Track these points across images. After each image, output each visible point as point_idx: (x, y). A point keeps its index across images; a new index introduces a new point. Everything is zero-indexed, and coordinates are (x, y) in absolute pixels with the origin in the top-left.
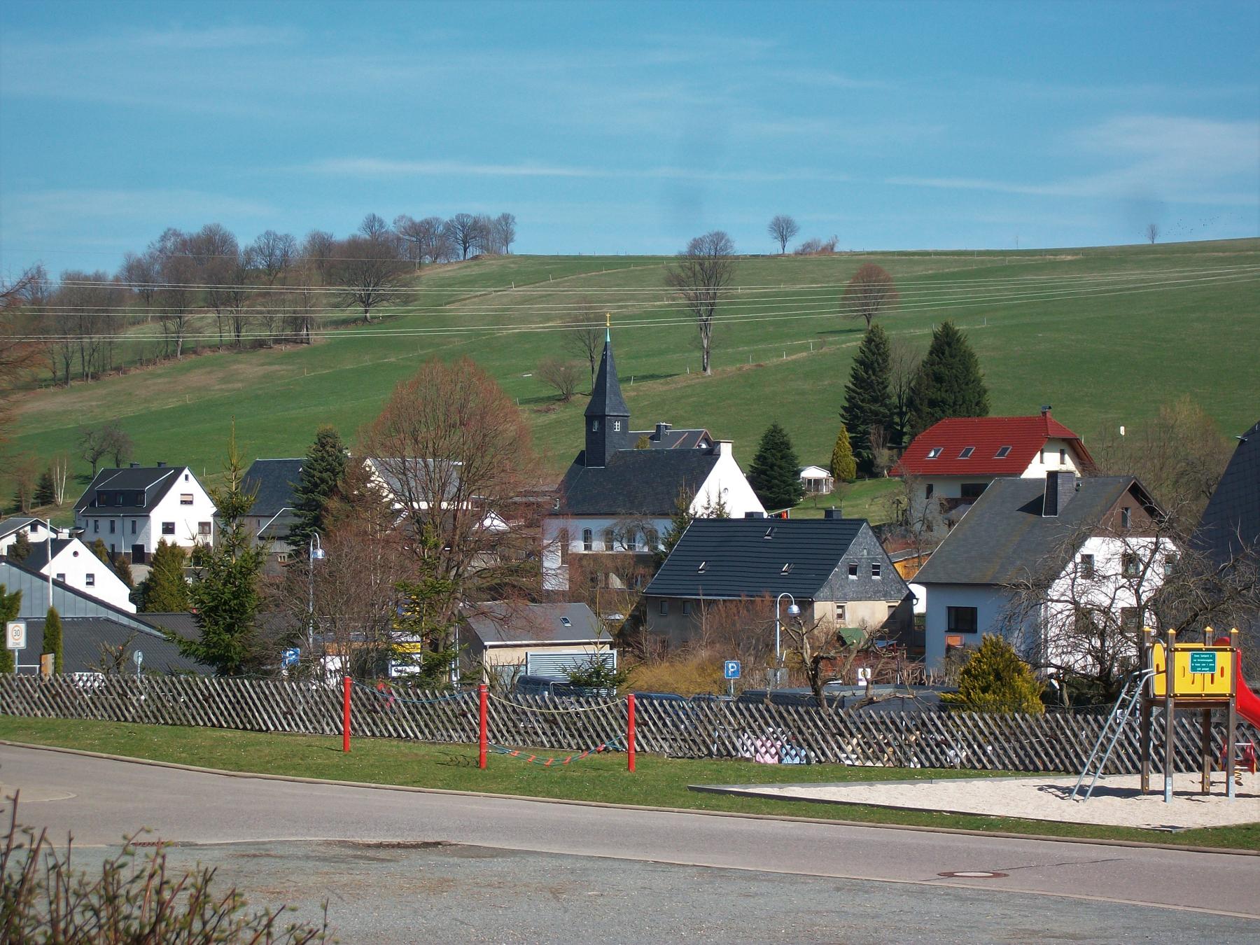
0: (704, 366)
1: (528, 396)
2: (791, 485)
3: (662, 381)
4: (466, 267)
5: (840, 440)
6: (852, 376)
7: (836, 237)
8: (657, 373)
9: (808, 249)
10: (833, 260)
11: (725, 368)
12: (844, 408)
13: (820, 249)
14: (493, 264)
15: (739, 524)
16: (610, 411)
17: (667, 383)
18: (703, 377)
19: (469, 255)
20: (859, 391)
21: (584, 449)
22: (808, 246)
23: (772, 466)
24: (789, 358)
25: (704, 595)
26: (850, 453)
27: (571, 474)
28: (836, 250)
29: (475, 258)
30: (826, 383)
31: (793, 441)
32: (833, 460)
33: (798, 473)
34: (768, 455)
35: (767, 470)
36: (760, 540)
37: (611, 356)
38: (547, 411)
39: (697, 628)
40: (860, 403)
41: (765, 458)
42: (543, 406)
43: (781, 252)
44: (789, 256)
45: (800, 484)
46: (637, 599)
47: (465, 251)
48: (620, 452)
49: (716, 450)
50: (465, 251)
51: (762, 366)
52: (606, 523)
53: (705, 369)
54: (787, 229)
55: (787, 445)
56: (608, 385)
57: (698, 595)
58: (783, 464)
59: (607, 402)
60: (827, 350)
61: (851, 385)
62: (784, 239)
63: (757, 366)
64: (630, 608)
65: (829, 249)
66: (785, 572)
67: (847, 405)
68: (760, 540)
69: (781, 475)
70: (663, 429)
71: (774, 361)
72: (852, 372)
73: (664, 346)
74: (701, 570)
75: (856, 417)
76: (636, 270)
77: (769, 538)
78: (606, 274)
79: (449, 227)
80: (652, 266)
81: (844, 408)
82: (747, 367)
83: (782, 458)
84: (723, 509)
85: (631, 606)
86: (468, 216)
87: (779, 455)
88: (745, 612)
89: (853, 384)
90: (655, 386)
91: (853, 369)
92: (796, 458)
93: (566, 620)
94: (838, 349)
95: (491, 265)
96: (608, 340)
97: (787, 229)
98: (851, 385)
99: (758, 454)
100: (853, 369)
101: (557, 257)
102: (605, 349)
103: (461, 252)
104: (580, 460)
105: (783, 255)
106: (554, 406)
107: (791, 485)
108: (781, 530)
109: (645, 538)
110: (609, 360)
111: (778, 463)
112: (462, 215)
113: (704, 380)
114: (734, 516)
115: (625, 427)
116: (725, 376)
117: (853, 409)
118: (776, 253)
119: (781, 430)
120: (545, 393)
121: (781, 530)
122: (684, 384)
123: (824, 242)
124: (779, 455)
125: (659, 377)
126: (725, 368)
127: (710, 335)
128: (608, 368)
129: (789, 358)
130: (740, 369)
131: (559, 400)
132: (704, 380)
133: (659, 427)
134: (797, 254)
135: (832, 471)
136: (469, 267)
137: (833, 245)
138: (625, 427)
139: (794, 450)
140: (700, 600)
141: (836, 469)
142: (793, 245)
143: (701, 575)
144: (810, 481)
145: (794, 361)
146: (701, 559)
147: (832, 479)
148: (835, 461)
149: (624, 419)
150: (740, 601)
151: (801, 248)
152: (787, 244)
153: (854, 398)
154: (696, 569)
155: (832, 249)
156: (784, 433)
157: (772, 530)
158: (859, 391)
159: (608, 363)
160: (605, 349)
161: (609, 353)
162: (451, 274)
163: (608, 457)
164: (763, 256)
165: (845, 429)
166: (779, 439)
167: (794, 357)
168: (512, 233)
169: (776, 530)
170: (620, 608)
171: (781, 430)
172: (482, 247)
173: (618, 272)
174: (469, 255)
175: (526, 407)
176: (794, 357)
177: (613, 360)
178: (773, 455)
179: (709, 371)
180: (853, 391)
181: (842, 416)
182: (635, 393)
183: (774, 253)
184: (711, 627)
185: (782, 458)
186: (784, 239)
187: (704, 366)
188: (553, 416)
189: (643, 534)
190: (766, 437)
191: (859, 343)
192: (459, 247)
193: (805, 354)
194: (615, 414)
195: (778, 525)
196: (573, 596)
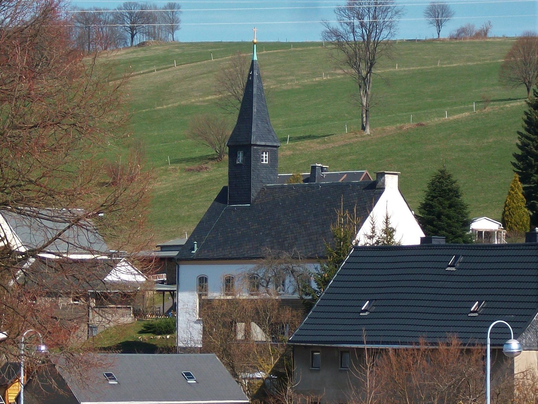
0: (363, 125)
1: (179, 157)
2: (460, 236)
3: (319, 140)
4: (132, 52)
5: (513, 190)
6: (526, 122)
7: (490, 22)
8: (314, 134)
9: (463, 34)
10: (487, 42)
11: (385, 128)
12: (517, 156)
13: (474, 34)
14: (157, 50)
15: (413, 252)
16: (256, 140)
17: (325, 142)
18: (362, 137)
19: (136, 42)
20: (532, 137)
21: (227, 184)
22: (463, 31)
23: (439, 216)
24: (451, 118)
25: (368, 343)
26: (523, 205)
27: (212, 212)
28: (489, 35)
29: (142, 44)
30: (491, 140)
31: (462, 189)
32: (504, 212)
33: (467, 224)
34: (435, 203)
35: (433, 220)
36: (441, 272)
37: (259, 77)
38: (200, 170)
39: (359, 385)
40: (534, 150)
41: (431, 206)
42: (196, 165)
43: (436, 37)
44: (443, 41)
45: (470, 236)
46: (281, 350)
47: (132, 37)
48: (268, 188)
49: (380, 184)
50: (132, 37)
51: (422, 125)
52: (248, 268)
53: (364, 128)
54: (442, 14)
55: (456, 193)
56: (255, 110)
57: (362, 343)
58: (452, 212)
59: (254, 130)
60: (491, 110)
61: (525, 132)
62: (439, 24)
63: (418, 125)
64: (273, 361)
65: (483, 34)
66: (474, 312)
67: (519, 152)
68: (441, 272)
69: (449, 226)
70: (318, 171)
71: (434, 121)
72: (525, 117)
73: (322, 116)
74: (365, 311)
75: (531, 166)
76: (296, 51)
77: (453, 269)
78: (266, 54)
79: (118, 18)
80: (311, 48)
81: (517, 156)
82: (407, 126)
83: (450, 206)
84: (392, 237)
85: (275, 359)
86: (136, 4)
87: (447, 203)
88: (424, 362)
89: (526, 130)
90: (312, 145)
91: (526, 113)
92: (465, 207)
93: (189, 376)
94: (502, 109)
95: (157, 50)
96: (255, 58)
97: (442, 14)
98: (525, 132)
99: (424, 202)
100: (526, 113)
101: (221, 43)
102: (252, 69)
103: (129, 41)
104: (222, 197)
105: (438, 39)
106: (206, 165)
107: (460, 236)
108: (468, 259)
109: (295, 283)
110: (255, 81)
111: (446, 211)
112: (130, 3)
113: (363, 139)
114: (405, 243)
115: (274, 159)
116: (385, 135)
117: (526, 157)
118: (432, 37)
119: (449, 176)
120: (197, 153)
121: (468, 259)
122: (342, 143)
123: (478, 27)
124: (447, 203)
125: (314, 137)
126: (385, 128)
127: (369, 92)
128: (255, 90)
129: (451, 118)
130: (401, 128)
131: (213, 159)
132: (363, 139)
133: (314, 168)
134: (451, 38)
135: (504, 223)
136: (135, 52)
137: (487, 30)
138: (274, 159)
139: (465, 199)
140: (363, 349)
141: (508, 221)
142: (447, 32)
143: (364, 318)
144: (480, 233)
145: (457, 121)
146: (363, 297)
147: (504, 233)
148: (507, 213)
149: (273, 150)
150: (418, 350)
151: (455, 33)
152: (443, 29)
153: (527, 145)
154: (356, 310)
155: (486, 34)
156: (453, 179)
157: (456, 259)
158: (532, 137)
159: (255, 85)
160: (252, 69)
161: (256, 73)
162: (119, 58)
163: (254, 194)
164: (418, 40)
165: (517, 179)
166: (447, 186)
167: (456, 117)
168: (178, 21)
169: (461, 259)
170: (260, 361)
171: (449, 176)
172: (149, 34)
173: (278, 52)
174: (136, 42)
175: (178, 166)
176: (456, 117)
177: (260, 81)
178: (441, 203)
179: (368, 131)
180: (527, 137)
181: (514, 165)
182: (292, 152)
183: (430, 37)
184: (378, 382)
185: (450, 206)
186: (439, 24)
187: (363, 125)
188: (205, 175)
189: (293, 279)
190: (433, 184)
191: (521, 103)
192: (126, 33)
193: (467, 114)
194: (263, 143)
195: (465, 252)
196: (206, 349)
